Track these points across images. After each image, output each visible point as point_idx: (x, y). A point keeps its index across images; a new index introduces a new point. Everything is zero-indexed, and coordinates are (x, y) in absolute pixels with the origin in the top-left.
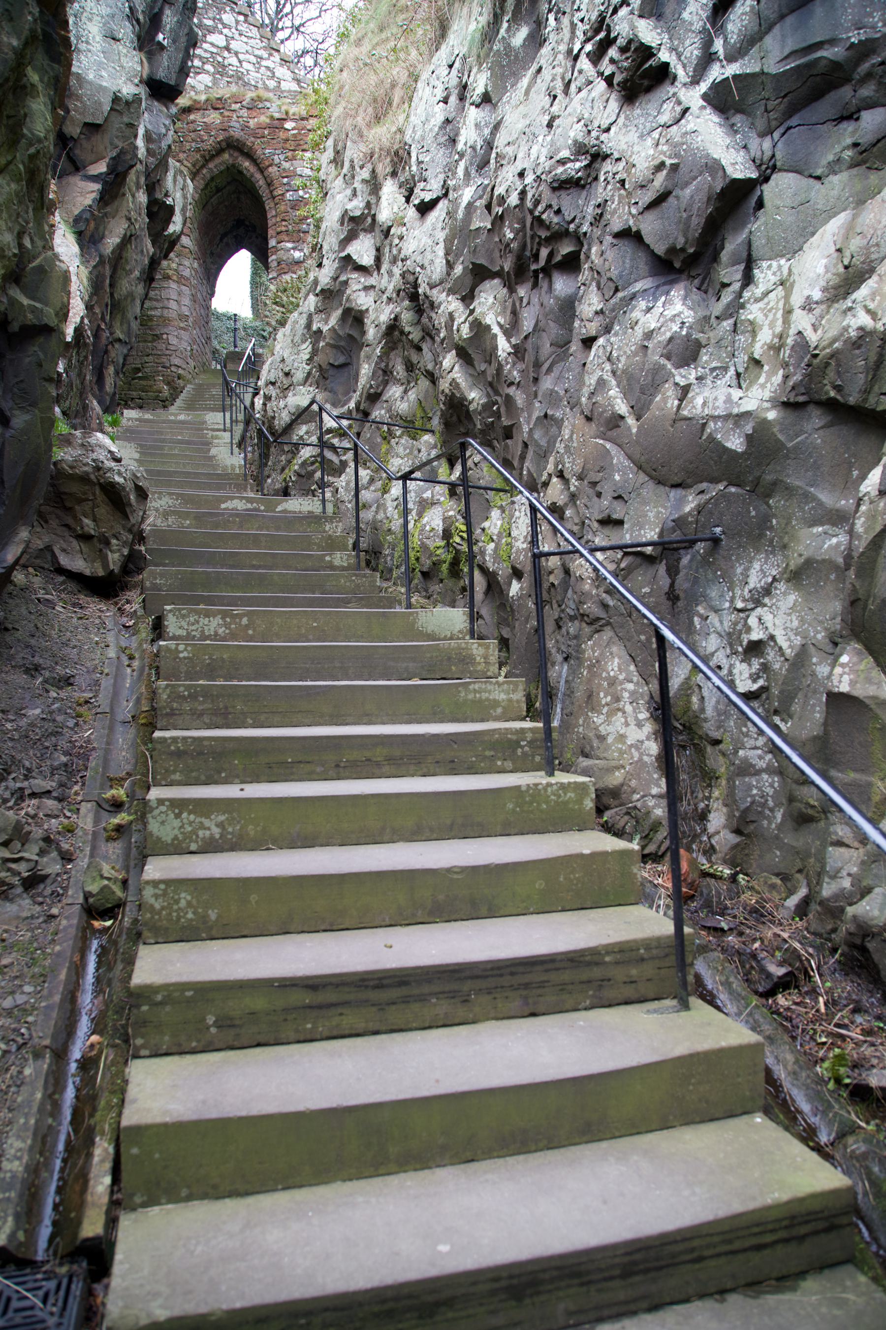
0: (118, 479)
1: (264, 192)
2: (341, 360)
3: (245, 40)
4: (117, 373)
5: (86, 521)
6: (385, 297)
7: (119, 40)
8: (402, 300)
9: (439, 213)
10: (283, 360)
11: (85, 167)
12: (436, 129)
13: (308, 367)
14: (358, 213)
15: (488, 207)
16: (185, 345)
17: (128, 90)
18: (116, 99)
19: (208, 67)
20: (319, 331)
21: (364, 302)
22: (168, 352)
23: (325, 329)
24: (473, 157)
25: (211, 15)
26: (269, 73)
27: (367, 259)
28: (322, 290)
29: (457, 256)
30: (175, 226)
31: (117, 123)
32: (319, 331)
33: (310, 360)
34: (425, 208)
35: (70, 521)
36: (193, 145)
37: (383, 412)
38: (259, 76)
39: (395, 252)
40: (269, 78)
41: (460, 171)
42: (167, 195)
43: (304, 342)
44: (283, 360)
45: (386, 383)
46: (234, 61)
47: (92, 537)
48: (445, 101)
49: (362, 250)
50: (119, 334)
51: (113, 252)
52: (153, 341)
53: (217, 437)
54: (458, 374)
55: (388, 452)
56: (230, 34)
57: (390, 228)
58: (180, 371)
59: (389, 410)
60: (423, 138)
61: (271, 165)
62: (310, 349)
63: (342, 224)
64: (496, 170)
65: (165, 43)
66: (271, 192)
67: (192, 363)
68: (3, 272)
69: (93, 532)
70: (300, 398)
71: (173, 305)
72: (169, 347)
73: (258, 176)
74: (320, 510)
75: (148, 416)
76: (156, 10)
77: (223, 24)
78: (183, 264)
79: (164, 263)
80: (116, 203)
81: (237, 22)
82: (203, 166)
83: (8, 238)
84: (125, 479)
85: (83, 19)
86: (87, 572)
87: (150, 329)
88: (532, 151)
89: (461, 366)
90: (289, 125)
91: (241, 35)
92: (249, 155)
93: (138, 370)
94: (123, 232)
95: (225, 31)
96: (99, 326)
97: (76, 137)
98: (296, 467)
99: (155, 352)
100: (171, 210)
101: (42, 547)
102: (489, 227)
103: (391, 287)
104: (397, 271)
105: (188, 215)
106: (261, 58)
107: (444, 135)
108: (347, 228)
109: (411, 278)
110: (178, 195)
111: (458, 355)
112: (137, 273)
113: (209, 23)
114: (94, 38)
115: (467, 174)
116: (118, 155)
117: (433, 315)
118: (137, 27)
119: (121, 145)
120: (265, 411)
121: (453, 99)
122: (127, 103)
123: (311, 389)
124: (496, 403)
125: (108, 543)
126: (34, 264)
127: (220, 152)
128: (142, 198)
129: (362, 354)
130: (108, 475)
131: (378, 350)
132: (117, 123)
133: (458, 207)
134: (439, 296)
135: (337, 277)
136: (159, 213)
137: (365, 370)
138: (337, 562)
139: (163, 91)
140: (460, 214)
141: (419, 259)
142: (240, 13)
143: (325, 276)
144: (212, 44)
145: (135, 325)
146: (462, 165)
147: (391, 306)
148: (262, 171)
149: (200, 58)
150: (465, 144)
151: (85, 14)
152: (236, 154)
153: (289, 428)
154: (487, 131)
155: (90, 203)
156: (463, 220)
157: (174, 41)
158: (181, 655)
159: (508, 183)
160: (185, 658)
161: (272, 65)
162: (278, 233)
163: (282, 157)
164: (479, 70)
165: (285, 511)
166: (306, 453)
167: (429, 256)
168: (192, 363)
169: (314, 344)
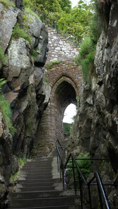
1: (74, 86)
3: (66, 47)
7: (23, 54)
11: (14, 89)
13: (79, 140)
16: (54, 134)
18: (22, 69)
20: (81, 127)
24: (107, 64)
25: (56, 43)
31: (23, 75)
32: (81, 127)
38: (71, 55)
43: (77, 131)
44: (71, 138)
46: (63, 53)
50: (28, 135)
51: (24, 111)
56: (62, 46)
58: (53, 143)
61: (76, 78)
65: (39, 52)
66: (76, 86)
71: (49, 123)
72: (49, 136)
73: (72, 82)
76: (36, 45)
78: (52, 110)
80: (25, 97)
81: (63, 43)
85: (13, 51)
89: (112, 137)
91: (64, 46)
94: (27, 105)
95: (60, 46)
96: (20, 134)
100: (44, 96)
106: (71, 51)
113: (56, 45)
114: (16, 55)
116: (23, 84)
118: (29, 50)
122: (26, 70)
128: (34, 94)
133: (105, 81)
135: (84, 109)
136: (40, 97)
142: (64, 41)
144: (57, 50)
148: (73, 81)
149: (54, 54)
150: (105, 61)
151: (13, 50)
152: (65, 77)
155: (15, 98)
157: (42, 51)
161: (74, 52)
169: (80, 132)
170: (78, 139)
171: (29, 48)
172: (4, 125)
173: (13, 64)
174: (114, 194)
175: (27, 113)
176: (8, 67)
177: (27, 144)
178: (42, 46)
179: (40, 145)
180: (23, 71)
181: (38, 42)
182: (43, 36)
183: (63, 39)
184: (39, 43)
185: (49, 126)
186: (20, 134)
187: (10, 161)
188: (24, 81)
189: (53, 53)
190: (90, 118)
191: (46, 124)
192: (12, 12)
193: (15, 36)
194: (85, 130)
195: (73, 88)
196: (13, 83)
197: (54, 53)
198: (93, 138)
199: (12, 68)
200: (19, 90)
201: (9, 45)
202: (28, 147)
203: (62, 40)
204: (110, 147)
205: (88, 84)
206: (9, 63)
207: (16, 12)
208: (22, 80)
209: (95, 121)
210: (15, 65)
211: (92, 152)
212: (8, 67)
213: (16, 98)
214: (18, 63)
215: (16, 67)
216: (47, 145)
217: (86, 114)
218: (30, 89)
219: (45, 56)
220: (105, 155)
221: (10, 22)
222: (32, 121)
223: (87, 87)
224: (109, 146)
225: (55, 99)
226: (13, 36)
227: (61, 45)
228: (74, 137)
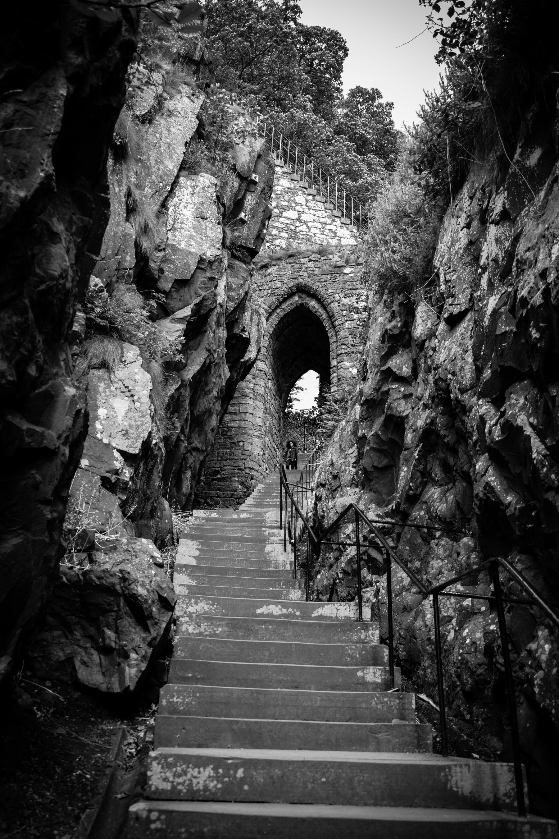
0: (141, 591)
3: (313, 212)
5: (109, 633)
6: (421, 403)
8: (437, 406)
9: (466, 325)
10: (332, 464)
11: (173, 312)
12: (461, 251)
14: (397, 332)
15: (512, 311)
17: (211, 253)
18: (201, 260)
19: (283, 234)
21: (403, 408)
22: (243, 457)
23: (369, 435)
24: (495, 269)
26: (332, 234)
27: (406, 370)
28: (366, 401)
29: (486, 361)
30: (251, 354)
31: (201, 278)
32: (364, 437)
34: (453, 321)
36: (270, 291)
37: (422, 513)
38: (324, 236)
39: (429, 362)
40: (332, 237)
41: (484, 283)
42: (243, 330)
44: (332, 464)
45: (424, 485)
48: (468, 226)
49: (400, 363)
50: (196, 443)
53: (273, 535)
54: (492, 478)
55: (427, 554)
56: (301, 210)
57: (424, 342)
58: (253, 473)
59: (428, 511)
60: (449, 260)
61: (333, 302)
62: (356, 453)
63: (383, 342)
64: (518, 275)
65: (246, 219)
66: (332, 323)
67: (265, 466)
69: (113, 645)
73: (321, 311)
74: (357, 616)
75: (214, 515)
76: (240, 197)
77: (296, 203)
78: (259, 383)
79: (243, 384)
81: (307, 201)
82: (277, 307)
84: (148, 591)
85: (180, 207)
88: (553, 251)
89: (494, 469)
91: (309, 209)
92: (314, 296)
93: (218, 472)
94: (203, 360)
95: (298, 208)
97: (168, 290)
98: (343, 565)
99: (232, 457)
100: (247, 342)
101: (63, 658)
102: (515, 330)
103: (427, 394)
104: (431, 378)
106: (326, 224)
107: (469, 255)
108: (386, 345)
109: (443, 385)
110: (254, 330)
111: (491, 458)
112: (215, 393)
113: (286, 203)
114: (187, 219)
115: (491, 284)
116: (201, 302)
117: (466, 419)
118: (222, 210)
119: (203, 293)
121: (475, 224)
122: (211, 263)
123: (357, 490)
124: (534, 508)
125: (126, 657)
126: (41, 390)
127: (291, 295)
128: (223, 333)
129: (402, 457)
131: (416, 454)
132: (201, 278)
134: (469, 399)
136: (237, 344)
137: (404, 472)
138: (369, 678)
139: (243, 253)
140: (486, 321)
142: (309, 194)
143: (368, 387)
144: (287, 218)
146: (485, 277)
147: (428, 411)
148: (324, 307)
149: (278, 228)
150: (488, 258)
151: (182, 204)
152: (304, 296)
154: (507, 244)
156: (489, 327)
157: (253, 217)
158: (153, 826)
159: (531, 285)
160: (157, 830)
161: (332, 227)
162: (338, 355)
163: (342, 295)
164: (497, 193)
165: (321, 617)
166: (351, 551)
167: (459, 363)
168: (265, 466)
169: (360, 449)
170: (352, 469)
171: (223, 205)
172: (153, 410)
173: (179, 245)
174: (490, 625)
175: (201, 382)
176: (164, 249)
177: (190, 467)
178: (255, 202)
179: (219, 476)
180: (203, 267)
181: (247, 190)
183: (306, 189)
184: (248, 194)
185: (248, 425)
186: (178, 437)
187: (156, 508)
189: (276, 224)
191: (239, 420)
192: (186, 99)
193: (188, 167)
195: (324, 327)
196: (172, 296)
198: (408, 467)
199: (174, 255)
200: (186, 317)
201: (171, 191)
202: (193, 477)
203: (304, 192)
204: (488, 497)
205: (398, 319)
206: (168, 238)
208: (200, 290)
209: (420, 423)
212: (164, 249)
214: (193, 243)
216: (238, 477)
217: (382, 401)
219: (261, 231)
220: (445, 519)
221: (180, 127)
222: (211, 405)
223: (395, 327)
224: (485, 494)
225: (270, 353)
226: (182, 168)
227: (301, 205)
228: (341, 461)
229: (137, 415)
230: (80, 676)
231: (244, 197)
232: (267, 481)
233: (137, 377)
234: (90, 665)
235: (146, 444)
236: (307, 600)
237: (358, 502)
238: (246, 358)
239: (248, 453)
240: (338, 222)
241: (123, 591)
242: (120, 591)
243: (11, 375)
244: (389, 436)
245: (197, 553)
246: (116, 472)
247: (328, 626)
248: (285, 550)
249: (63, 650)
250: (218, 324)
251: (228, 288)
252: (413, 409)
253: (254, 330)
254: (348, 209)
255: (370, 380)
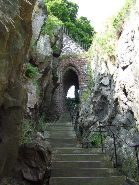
1: (77, 73)
2: (101, 108)
4: (45, 114)
5: (33, 162)
18: (46, 57)
19: (65, 51)
22: (57, 108)
30: (59, 81)
31: (46, 61)
32: (95, 102)
33: (93, 109)
35: (28, 162)
42: (57, 75)
45: (116, 114)
46: (70, 49)
47: (34, 167)
50: (46, 105)
52: (53, 106)
68: (1, 89)
69: (34, 166)
70: (91, 118)
71: (58, 98)
74: (101, 152)
78: (60, 89)
80: (46, 77)
81: (71, 43)
83: (4, 78)
86: (32, 179)
87: (53, 104)
90: (82, 60)
92: (74, 66)
97: (38, 65)
100: (58, 78)
101: (19, 171)
105: (61, 79)
110: (59, 75)
120: (81, 122)
122: (49, 57)
123: (94, 116)
125: (39, 170)
128: (52, 76)
129: (108, 107)
130: (40, 148)
136: (55, 79)
137: (110, 111)
138: (110, 172)
139: (56, 55)
141: (125, 81)
144: (66, 47)
145: (49, 103)
149: (64, 50)
152: (71, 66)
153: (89, 127)
155: (40, 77)
157: (58, 46)
161: (77, 49)
182: (61, 36)
184: (57, 40)
188: (47, 65)
190: (105, 95)
192: (41, 16)
194: (98, 104)
197: (64, 49)
201: (38, 39)
203: (70, 41)
207: (43, 17)
210: (41, 53)
211: (110, 121)
213: (41, 77)
215: (42, 55)
217: (100, 92)
218: (50, 72)
226: (40, 33)
229: (32, 97)
230: (24, 176)
231: (56, 41)
232: (63, 114)
233: (32, 87)
234: (27, 172)
235: (36, 106)
236: (82, 148)
237: (94, 119)
238: (57, 82)
239: (58, 107)
240: (79, 48)
241: (37, 149)
242: (36, 150)
243: (7, 81)
244: (102, 101)
245: (49, 135)
246: (28, 113)
247: (62, 147)
248: (73, 133)
249: (19, 168)
250: (51, 74)
251: (53, 64)
252: (111, 93)
253: (59, 75)
254: (81, 45)
255: (96, 86)
